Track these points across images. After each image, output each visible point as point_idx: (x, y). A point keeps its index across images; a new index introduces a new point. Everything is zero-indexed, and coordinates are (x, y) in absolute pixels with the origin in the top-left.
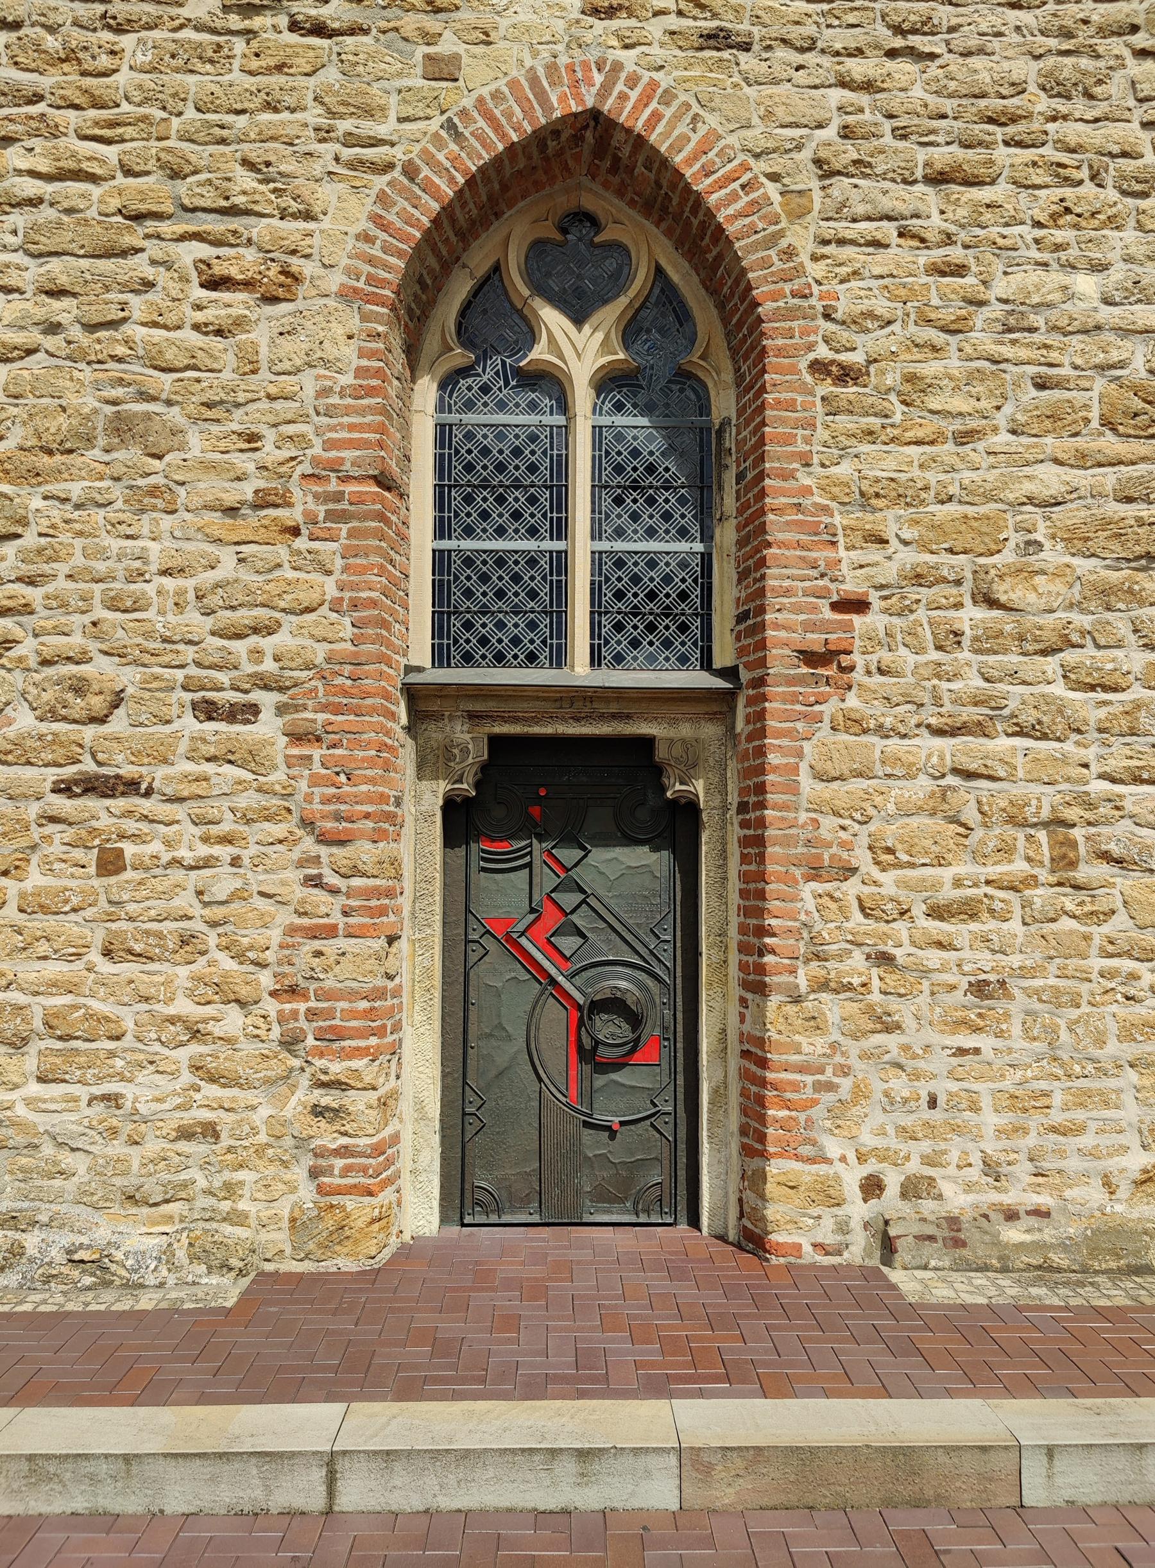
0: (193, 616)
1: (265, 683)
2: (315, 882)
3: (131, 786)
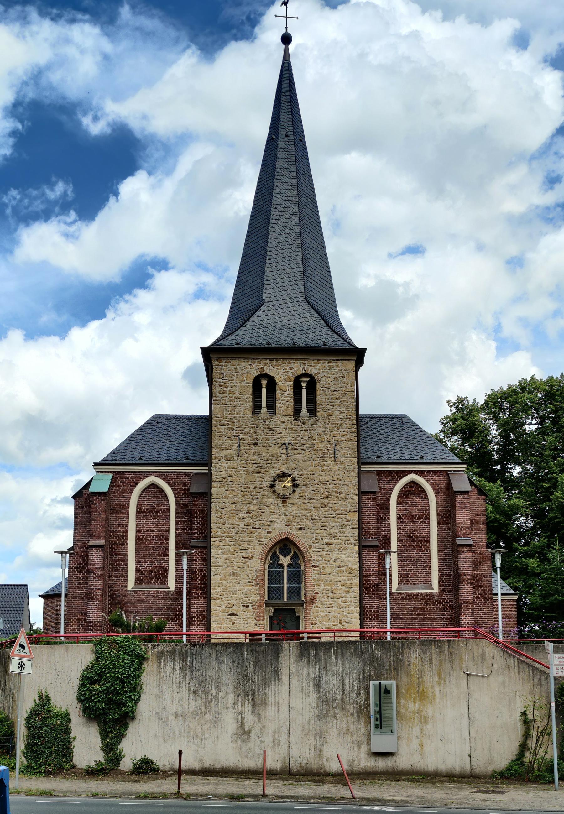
0: (242, 596)
1: (250, 603)
2: (256, 625)
3: (236, 615)
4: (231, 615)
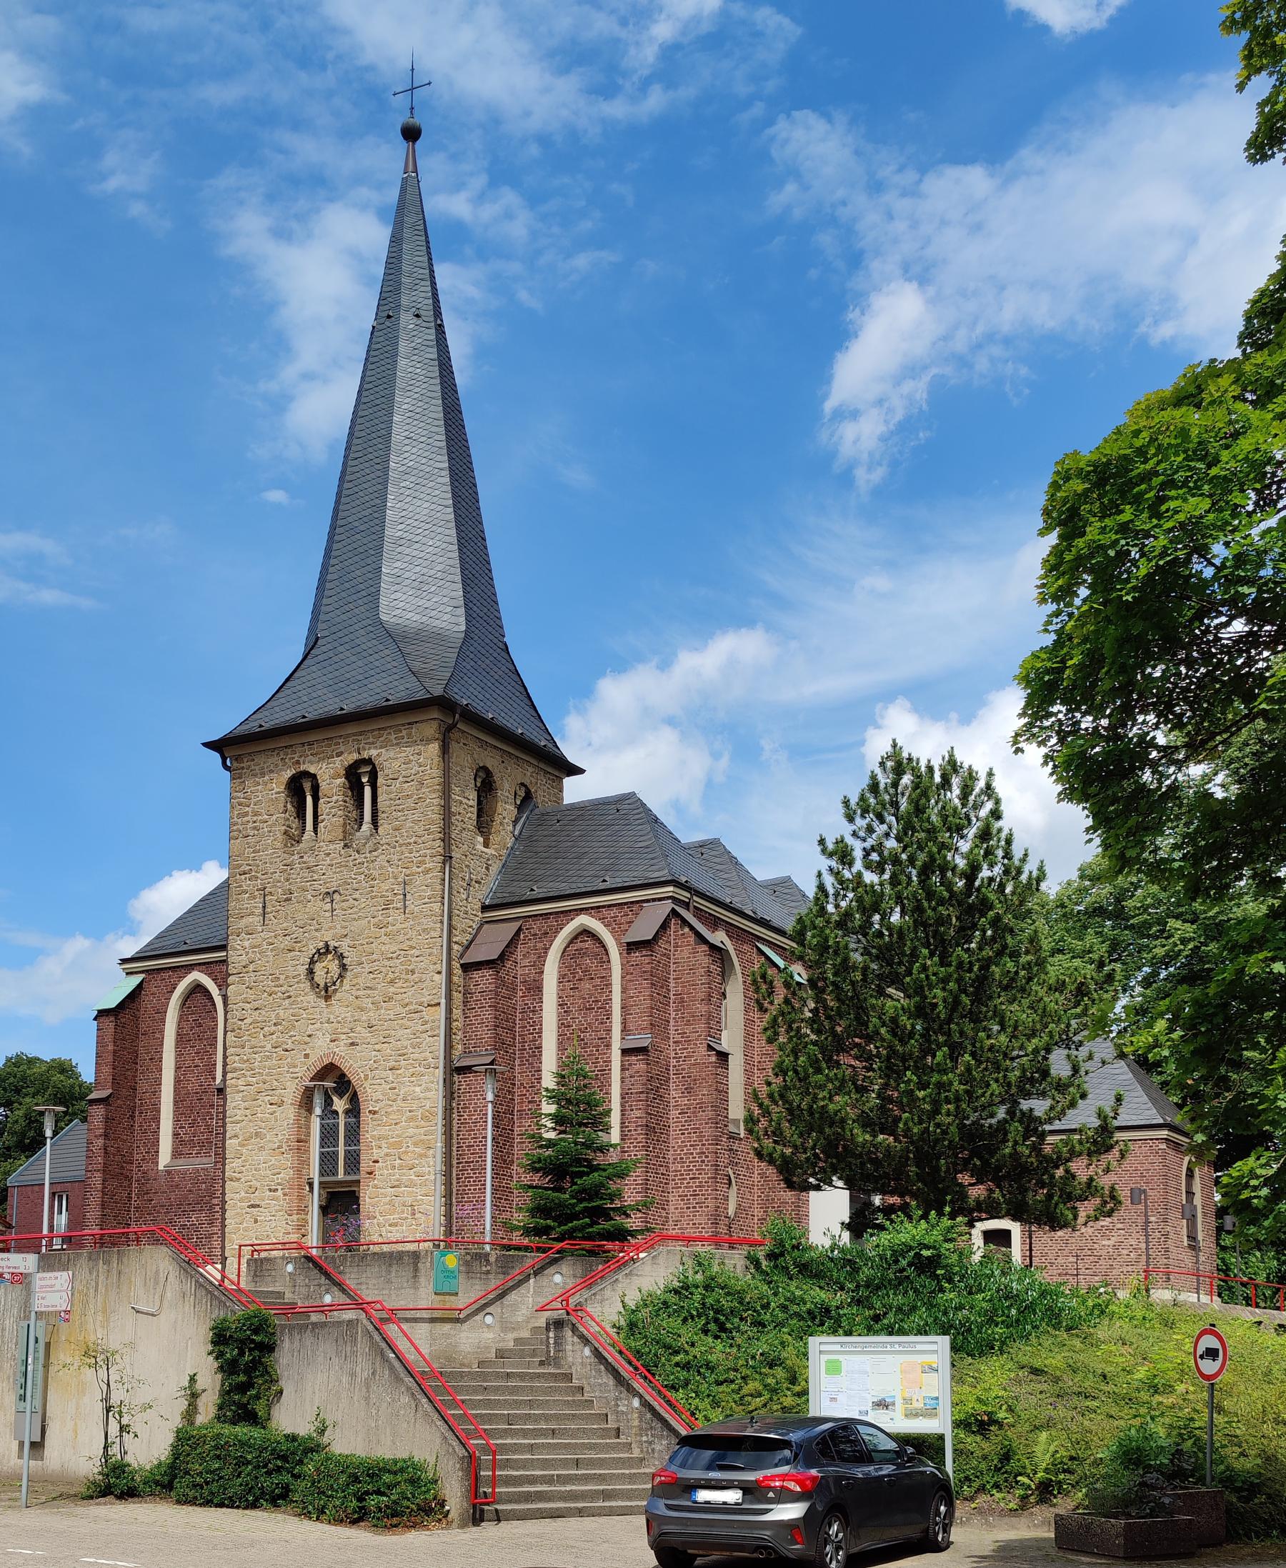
1: (279, 1184)
3: (259, 1206)
4: (253, 1206)
